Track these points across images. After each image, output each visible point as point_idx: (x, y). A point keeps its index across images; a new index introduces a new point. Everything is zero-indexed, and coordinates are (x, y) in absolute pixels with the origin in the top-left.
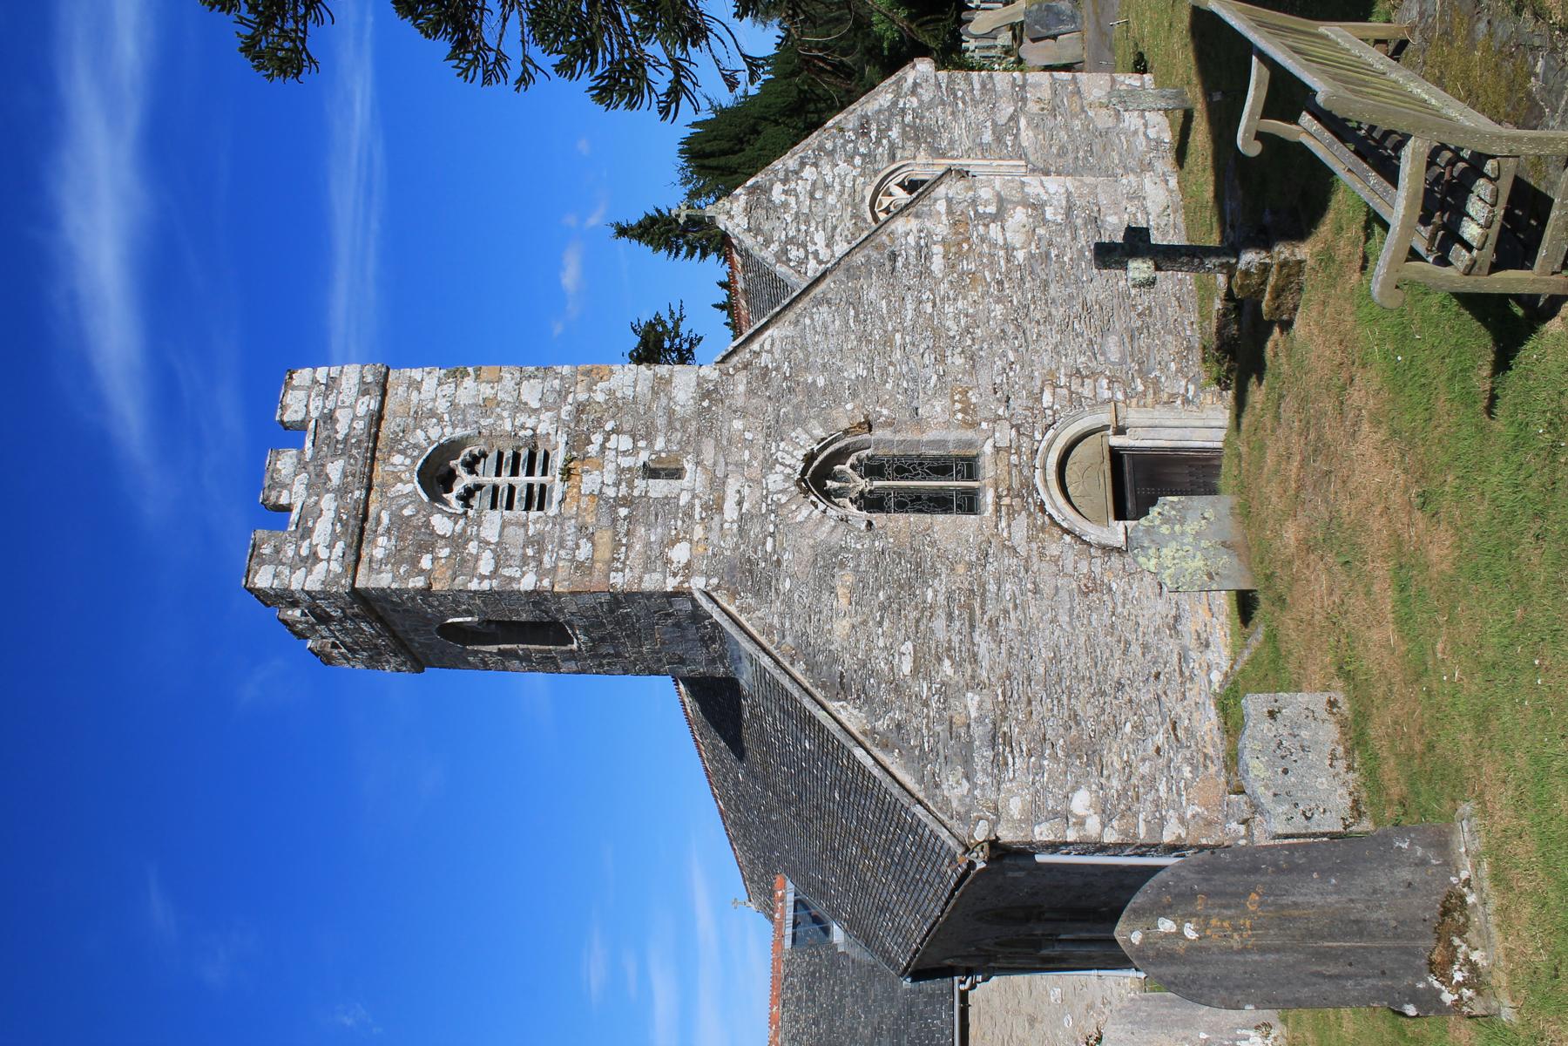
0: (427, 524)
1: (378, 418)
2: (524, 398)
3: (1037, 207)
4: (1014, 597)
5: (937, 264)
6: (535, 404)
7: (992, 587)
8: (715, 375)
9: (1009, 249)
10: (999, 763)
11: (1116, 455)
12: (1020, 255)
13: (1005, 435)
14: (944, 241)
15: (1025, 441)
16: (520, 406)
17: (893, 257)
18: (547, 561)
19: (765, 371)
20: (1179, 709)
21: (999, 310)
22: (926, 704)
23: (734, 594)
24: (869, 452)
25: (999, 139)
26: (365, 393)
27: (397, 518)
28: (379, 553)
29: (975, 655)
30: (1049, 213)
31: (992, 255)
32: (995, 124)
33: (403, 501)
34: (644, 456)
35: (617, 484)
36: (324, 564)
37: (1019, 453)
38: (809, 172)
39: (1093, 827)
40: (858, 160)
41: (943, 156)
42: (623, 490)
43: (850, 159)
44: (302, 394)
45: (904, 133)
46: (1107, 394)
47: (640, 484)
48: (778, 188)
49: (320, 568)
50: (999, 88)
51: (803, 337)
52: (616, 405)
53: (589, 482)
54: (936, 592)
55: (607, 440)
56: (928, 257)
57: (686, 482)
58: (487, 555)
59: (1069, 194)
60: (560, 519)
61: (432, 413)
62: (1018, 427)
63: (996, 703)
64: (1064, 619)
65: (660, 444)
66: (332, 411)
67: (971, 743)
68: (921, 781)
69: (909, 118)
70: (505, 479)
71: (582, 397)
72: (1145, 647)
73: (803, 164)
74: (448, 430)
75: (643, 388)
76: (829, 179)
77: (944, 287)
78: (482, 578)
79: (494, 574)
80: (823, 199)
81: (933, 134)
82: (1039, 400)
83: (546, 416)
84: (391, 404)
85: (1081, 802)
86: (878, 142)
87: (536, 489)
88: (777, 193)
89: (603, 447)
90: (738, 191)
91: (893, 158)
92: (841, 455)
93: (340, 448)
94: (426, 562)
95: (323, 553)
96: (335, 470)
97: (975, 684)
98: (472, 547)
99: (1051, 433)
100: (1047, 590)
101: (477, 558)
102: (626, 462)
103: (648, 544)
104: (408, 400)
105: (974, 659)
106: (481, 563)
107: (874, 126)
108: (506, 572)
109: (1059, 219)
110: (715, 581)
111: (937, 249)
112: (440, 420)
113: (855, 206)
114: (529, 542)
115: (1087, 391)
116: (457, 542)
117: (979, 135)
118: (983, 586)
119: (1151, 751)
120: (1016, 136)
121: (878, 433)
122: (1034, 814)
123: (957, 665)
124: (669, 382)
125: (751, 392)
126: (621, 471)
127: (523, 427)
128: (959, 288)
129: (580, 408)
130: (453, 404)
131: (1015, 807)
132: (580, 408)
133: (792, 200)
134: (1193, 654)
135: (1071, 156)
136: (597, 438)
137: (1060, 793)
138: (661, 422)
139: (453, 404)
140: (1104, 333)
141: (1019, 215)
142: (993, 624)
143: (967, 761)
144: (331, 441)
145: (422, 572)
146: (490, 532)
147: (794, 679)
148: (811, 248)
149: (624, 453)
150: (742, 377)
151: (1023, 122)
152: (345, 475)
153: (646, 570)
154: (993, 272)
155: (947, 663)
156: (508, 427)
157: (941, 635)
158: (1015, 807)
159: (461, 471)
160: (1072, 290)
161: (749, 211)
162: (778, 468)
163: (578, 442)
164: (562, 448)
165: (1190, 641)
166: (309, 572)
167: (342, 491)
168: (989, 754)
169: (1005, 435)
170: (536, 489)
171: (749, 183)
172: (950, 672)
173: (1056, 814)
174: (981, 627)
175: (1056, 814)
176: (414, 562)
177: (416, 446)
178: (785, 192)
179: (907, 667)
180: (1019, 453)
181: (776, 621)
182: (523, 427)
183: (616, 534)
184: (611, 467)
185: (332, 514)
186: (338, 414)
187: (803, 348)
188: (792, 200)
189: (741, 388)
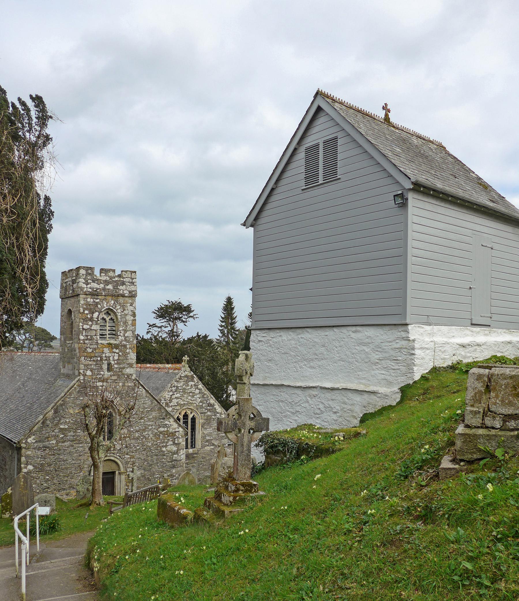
0: (96, 311)
1: (123, 296)
2: (128, 332)
3: (177, 453)
4: (78, 450)
5: (162, 429)
6: (126, 335)
7: (81, 445)
8: (133, 378)
9: (166, 446)
10: (39, 449)
11: (113, 473)
12: (164, 449)
13: (118, 447)
14: (168, 431)
15: (116, 452)
16: (125, 331)
17: (164, 419)
18: (87, 342)
19: (134, 390)
20: (52, 489)
21: (150, 444)
22: (53, 431)
23: (78, 386)
24: (114, 415)
25: (207, 441)
26: (130, 292)
27: (97, 304)
28: (89, 300)
29: (65, 442)
30: (176, 456)
31: (164, 442)
32: (212, 440)
33: (102, 305)
34: (113, 362)
35: (106, 357)
36: (86, 286)
37: (114, 450)
38: (197, 391)
39: (24, 470)
40: (201, 404)
41: (202, 427)
42: (104, 358)
43: (201, 402)
44: (130, 276)
45: (208, 416)
46: (128, 470)
47: (106, 362)
48: (193, 383)
49: (85, 286)
50: (223, 440)
51: (143, 398)
52: (126, 355)
53: (106, 350)
54: (79, 432)
55: (117, 353)
56: (164, 427)
57: (106, 373)
58: (88, 327)
59: (181, 460)
60: (97, 343)
61: (124, 310)
62: (120, 450)
63: (53, 447)
64: (73, 462)
65: (116, 366)
66: (125, 284)
67: (44, 442)
68: (35, 431)
69: (213, 417)
70: (108, 328)
71: (128, 346)
72: (67, 481)
73: (200, 389)
74: (120, 314)
75: (130, 361)
76: (195, 397)
77: (156, 431)
78: (83, 326)
79: (83, 329)
80: (190, 396)
81: (209, 424)
82: (127, 454)
83: (123, 338)
84: (127, 299)
85: (30, 467)
86: (206, 409)
87: (105, 336)
88: (191, 383)
89: (115, 352)
90: (192, 373)
91: (201, 413)
92: (114, 410)
93: (115, 287)
94: (86, 312)
95: (89, 286)
96: (110, 287)
97: (57, 442)
98: (90, 323)
99: (118, 457)
100: (80, 458)
101: (87, 324)
102: (111, 358)
103: (91, 365)
104: (127, 303)
105: (63, 442)
106: (86, 326)
107: (211, 408)
108: (84, 332)
109: (174, 458)
110: (82, 381)
111: (166, 429)
112: (122, 312)
113: (187, 404)
114: (91, 336)
115: (129, 465)
116: (91, 319)
117: (208, 436)
118: (81, 443)
119: (42, 483)
120: (208, 445)
121: (118, 417)
122: (27, 457)
123: (62, 438)
124: (131, 367)
125: (129, 387)
126: (109, 357)
127: (120, 332)
128: (155, 435)
129: (125, 346)
130: (126, 315)
131: (29, 453)
132: (125, 346)
133: (189, 387)
134: (65, 491)
135: (202, 460)
136: (117, 351)
137: (32, 463)
138: (121, 366)
139: (126, 315)
140: (144, 469)
141: (175, 449)
142: (72, 446)
143: (40, 441)
144: (117, 285)
145: (84, 311)
146: (94, 327)
147: (58, 401)
148: (175, 393)
149: (113, 358)
150: (133, 384)
151: (212, 447)
152: (109, 289)
153: (85, 365)
154: (160, 443)
155: (63, 436)
156: (120, 329)
157: (69, 434)
158: (29, 453)
159: (110, 317)
160: (155, 462)
161: (186, 376)
162: (110, 394)
163: (116, 346)
164: (115, 342)
165: (68, 491)
166: (84, 283)
167: (104, 289)
168: (41, 446)
169: (118, 447)
170: (105, 336)
171: (194, 376)
172: (61, 436)
173: (27, 462)
174: (71, 443)
175: (27, 462)
176: (86, 309)
177: (116, 306)
178: (192, 385)
179: (62, 427)
180: (114, 450)
181: (72, 396)
182: (120, 332)
183: (94, 357)
184: (110, 355)
185: (98, 287)
186: (125, 286)
187: (140, 399)
188: (189, 387)
189: (130, 384)
